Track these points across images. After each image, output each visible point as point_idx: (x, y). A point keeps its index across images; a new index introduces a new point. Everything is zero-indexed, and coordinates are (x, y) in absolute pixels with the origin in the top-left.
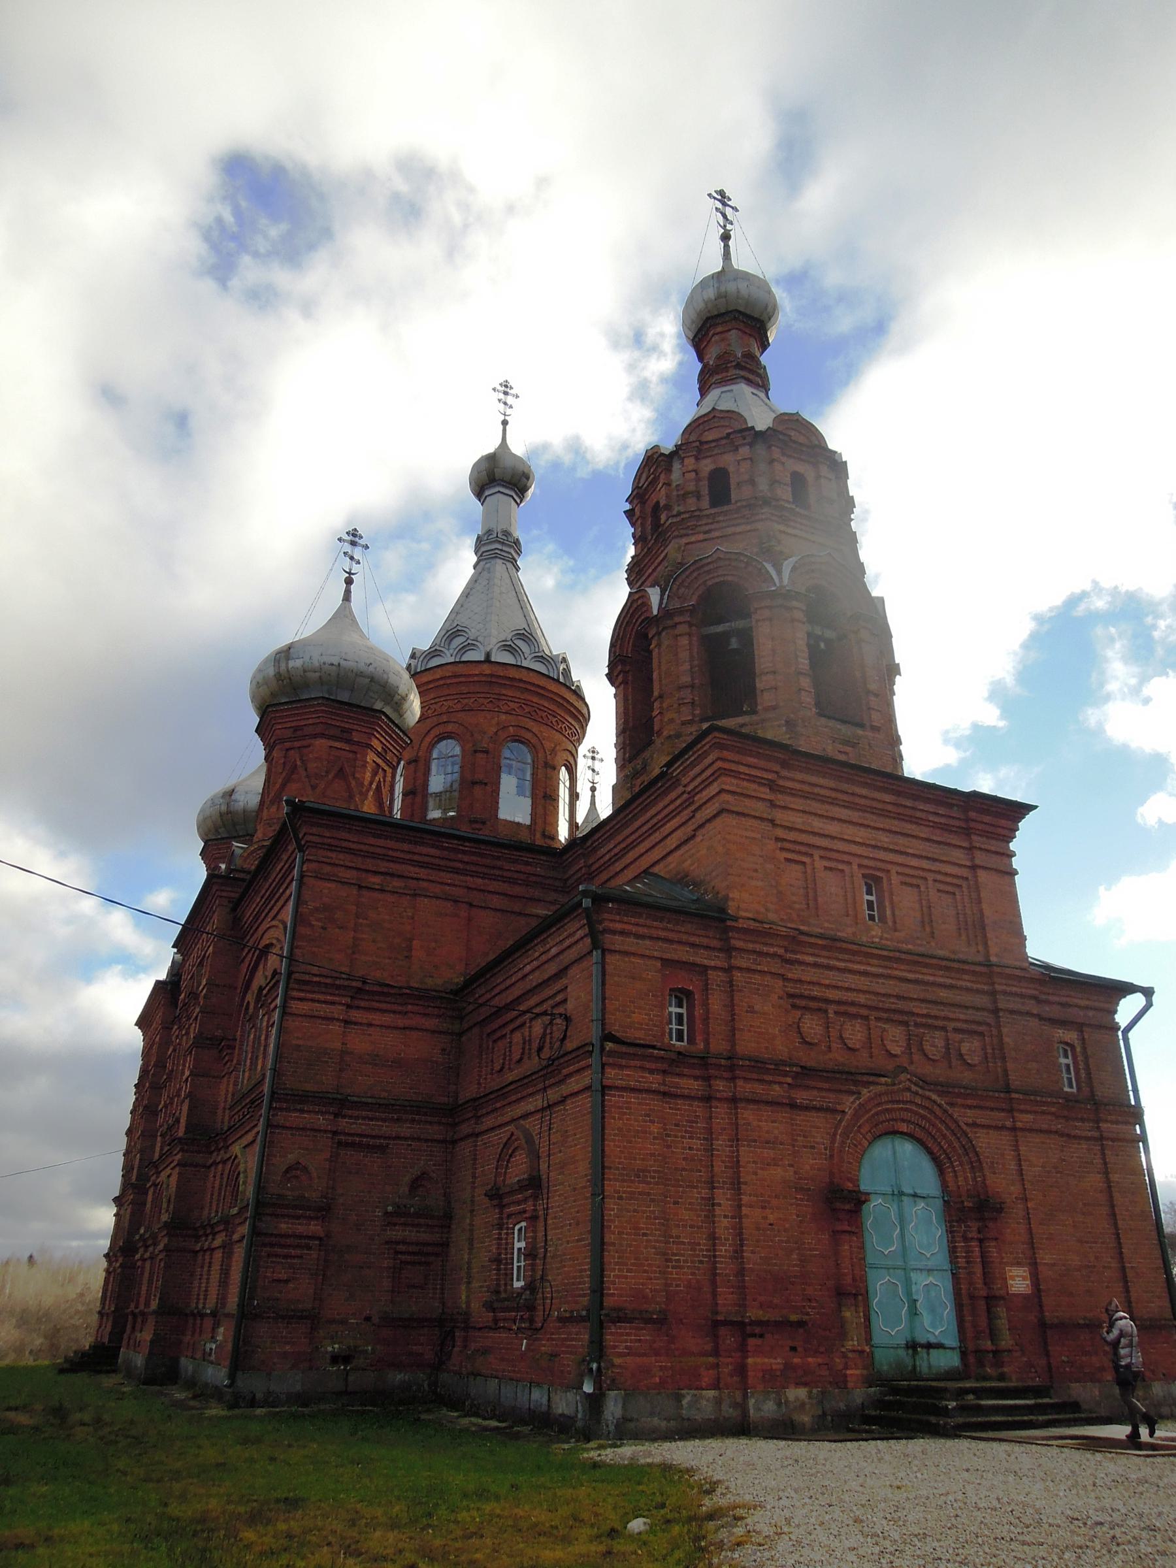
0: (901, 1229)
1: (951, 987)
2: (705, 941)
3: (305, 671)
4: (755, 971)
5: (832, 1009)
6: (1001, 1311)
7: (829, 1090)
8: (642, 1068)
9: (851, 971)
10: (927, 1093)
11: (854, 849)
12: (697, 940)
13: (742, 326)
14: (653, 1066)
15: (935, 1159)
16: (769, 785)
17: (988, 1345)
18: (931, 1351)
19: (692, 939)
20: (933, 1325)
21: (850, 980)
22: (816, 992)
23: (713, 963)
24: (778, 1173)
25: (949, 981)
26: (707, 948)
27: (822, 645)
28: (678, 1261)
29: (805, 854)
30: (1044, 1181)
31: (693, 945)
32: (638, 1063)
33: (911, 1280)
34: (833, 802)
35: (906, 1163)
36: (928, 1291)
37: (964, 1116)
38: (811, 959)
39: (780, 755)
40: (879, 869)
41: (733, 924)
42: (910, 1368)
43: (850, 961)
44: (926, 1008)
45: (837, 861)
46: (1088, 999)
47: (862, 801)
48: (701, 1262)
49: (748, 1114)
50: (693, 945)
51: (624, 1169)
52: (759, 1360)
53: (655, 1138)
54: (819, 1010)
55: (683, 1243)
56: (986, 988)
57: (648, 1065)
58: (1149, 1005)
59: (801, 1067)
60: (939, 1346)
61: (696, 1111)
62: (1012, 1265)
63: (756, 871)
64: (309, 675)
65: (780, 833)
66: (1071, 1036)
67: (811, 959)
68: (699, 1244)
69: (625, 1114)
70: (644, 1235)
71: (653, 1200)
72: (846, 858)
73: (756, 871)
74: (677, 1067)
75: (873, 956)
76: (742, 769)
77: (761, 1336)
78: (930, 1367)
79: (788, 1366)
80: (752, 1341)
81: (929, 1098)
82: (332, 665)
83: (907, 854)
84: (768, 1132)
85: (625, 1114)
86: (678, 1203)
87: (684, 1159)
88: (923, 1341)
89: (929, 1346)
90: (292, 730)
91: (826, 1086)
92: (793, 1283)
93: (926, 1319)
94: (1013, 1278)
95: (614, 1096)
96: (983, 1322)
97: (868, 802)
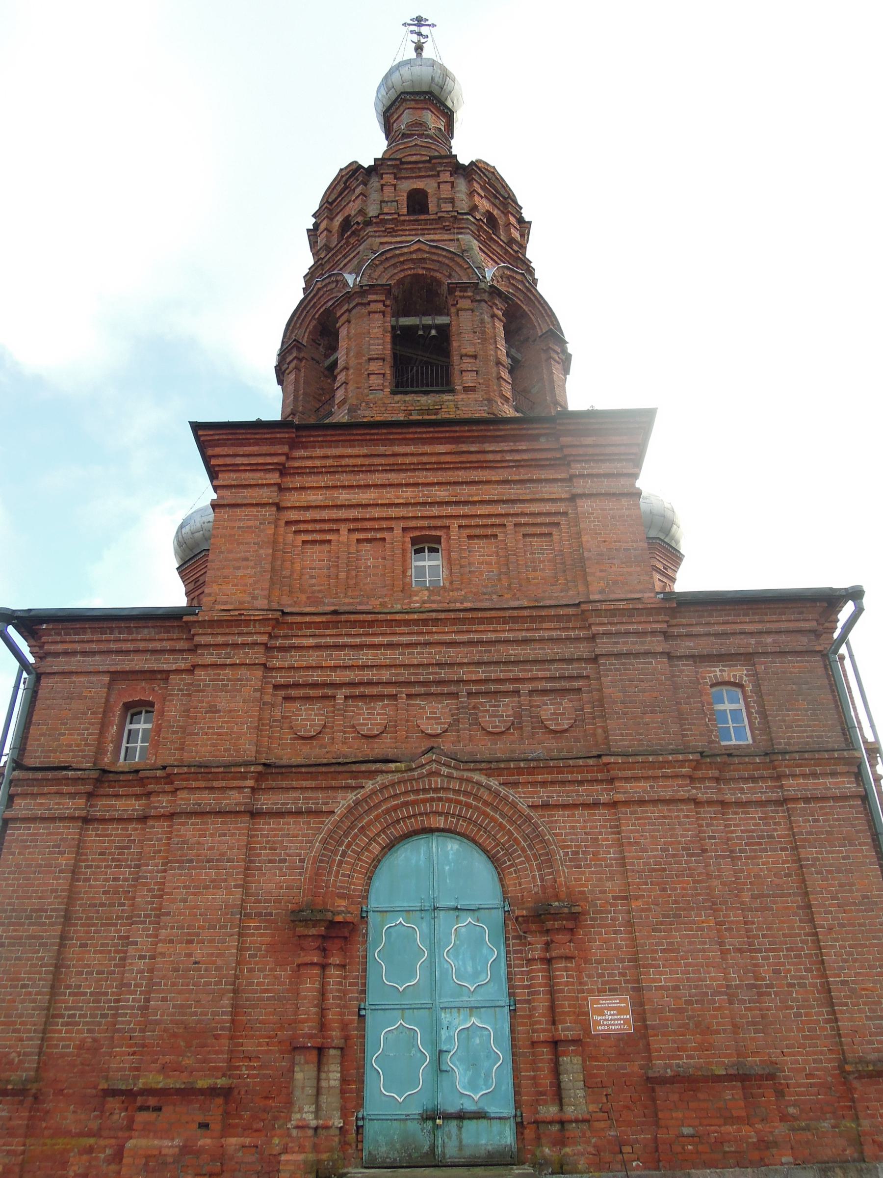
0: (430, 955)
1: (525, 641)
2: (167, 645)
3: (192, 534)
4: (224, 666)
5: (340, 694)
6: (572, 1064)
7: (316, 789)
8: (60, 794)
9: (344, 646)
10: (466, 774)
11: (392, 512)
12: (158, 645)
13: (413, 104)
14: (72, 789)
15: (493, 859)
16: (279, 470)
17: (550, 1111)
18: (466, 1122)
19: (151, 646)
20: (473, 1085)
21: (366, 657)
22: (317, 677)
23: (174, 667)
24: (220, 896)
25: (520, 635)
26: (172, 651)
27: (433, 332)
28: (74, 1016)
29: (331, 531)
30: (664, 870)
31: (154, 652)
32: (54, 789)
33: (441, 1023)
34: (370, 470)
35: (447, 868)
36: (468, 1038)
37: (521, 798)
38: (311, 641)
39: (282, 435)
40: (436, 528)
41: (192, 618)
42: (426, 1148)
43: (367, 635)
44: (483, 672)
45: (375, 530)
46: (760, 622)
47: (408, 460)
48: (104, 1016)
49: (188, 830)
50: (154, 652)
51: (13, 910)
52: (143, 1142)
53: (61, 871)
54: (325, 697)
55: (85, 994)
56: (582, 634)
57: (65, 789)
58: (859, 611)
59: (264, 765)
60: (480, 1115)
61: (131, 835)
62: (601, 991)
63: (247, 559)
64: (196, 535)
65: (293, 515)
66: (739, 673)
67: (311, 641)
68: (106, 994)
69: (29, 847)
70: (24, 986)
71: (44, 945)
72: (384, 524)
73: (247, 559)
74: (109, 787)
75: (399, 623)
76: (239, 460)
77: (158, 1109)
78: (461, 1147)
79: (185, 1150)
80: (142, 1117)
81: (469, 780)
82: (209, 522)
83: (474, 503)
84: (211, 848)
85: (29, 847)
86: (85, 945)
87: (104, 893)
88: (452, 1109)
89: (461, 1116)
90: (193, 583)
91: (313, 784)
92: (217, 1037)
93: (460, 1076)
94: (600, 1012)
95: (19, 829)
96: (546, 1081)
97: (415, 460)
